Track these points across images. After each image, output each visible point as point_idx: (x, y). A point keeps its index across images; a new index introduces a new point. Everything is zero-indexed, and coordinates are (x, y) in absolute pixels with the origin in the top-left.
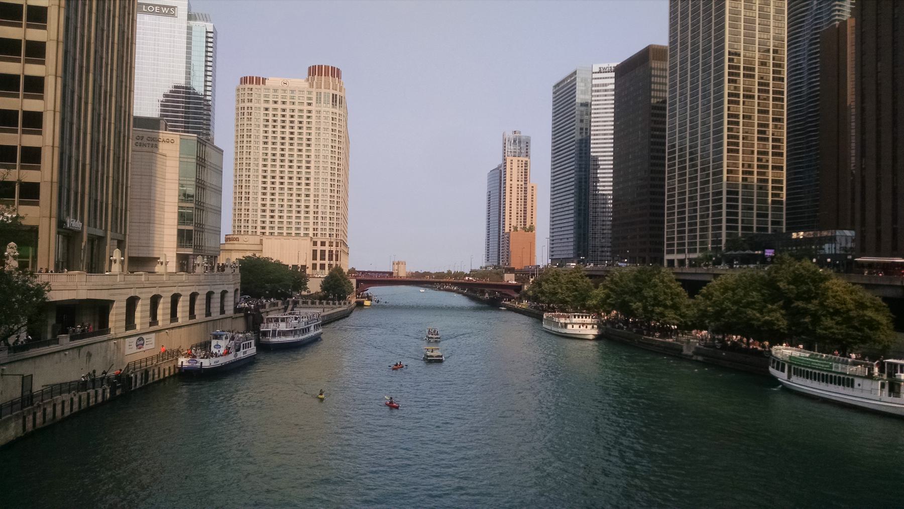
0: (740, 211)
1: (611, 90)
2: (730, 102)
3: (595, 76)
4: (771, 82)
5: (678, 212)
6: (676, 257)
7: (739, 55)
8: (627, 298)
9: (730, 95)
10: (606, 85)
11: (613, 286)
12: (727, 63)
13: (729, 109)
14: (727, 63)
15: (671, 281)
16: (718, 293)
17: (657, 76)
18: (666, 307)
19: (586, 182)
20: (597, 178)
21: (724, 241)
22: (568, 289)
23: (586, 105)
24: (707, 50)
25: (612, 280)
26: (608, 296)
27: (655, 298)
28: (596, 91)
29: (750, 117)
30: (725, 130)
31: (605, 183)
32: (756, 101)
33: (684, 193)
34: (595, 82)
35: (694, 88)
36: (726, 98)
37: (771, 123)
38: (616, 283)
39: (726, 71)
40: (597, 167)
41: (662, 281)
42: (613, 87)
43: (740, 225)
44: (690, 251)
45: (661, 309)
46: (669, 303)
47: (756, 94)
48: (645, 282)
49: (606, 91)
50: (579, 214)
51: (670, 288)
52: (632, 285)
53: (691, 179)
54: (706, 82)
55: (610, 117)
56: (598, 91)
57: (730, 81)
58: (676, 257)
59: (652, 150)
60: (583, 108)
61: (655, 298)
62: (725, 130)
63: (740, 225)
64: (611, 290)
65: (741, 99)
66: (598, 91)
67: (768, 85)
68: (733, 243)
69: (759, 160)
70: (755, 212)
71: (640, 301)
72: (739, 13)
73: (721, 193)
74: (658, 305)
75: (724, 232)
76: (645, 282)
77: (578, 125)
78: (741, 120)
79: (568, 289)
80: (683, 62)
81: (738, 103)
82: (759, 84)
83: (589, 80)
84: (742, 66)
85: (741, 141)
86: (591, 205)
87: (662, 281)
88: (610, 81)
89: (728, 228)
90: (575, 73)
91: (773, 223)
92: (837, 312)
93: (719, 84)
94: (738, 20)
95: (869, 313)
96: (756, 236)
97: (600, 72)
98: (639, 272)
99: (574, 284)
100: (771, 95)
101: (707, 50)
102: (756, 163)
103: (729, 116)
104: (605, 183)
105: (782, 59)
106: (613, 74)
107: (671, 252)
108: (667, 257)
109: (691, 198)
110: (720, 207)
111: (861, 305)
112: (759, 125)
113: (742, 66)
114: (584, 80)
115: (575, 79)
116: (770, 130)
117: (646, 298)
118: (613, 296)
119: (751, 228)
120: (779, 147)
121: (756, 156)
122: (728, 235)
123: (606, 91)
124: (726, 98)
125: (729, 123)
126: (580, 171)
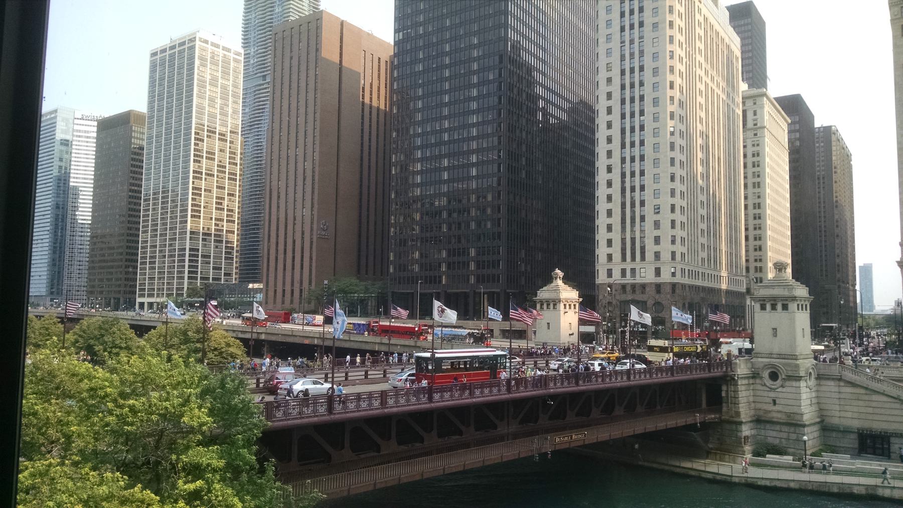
0: (199, 264)
1: (93, 138)
2: (194, 177)
3: (76, 121)
4: (227, 165)
5: (170, 239)
6: (146, 300)
7: (203, 141)
8: (92, 342)
9: (194, 172)
10: (88, 132)
11: (82, 333)
12: (193, 147)
13: (193, 183)
14: (193, 147)
15: (126, 330)
16: (154, 339)
17: (137, 138)
18: (121, 348)
19: (63, 221)
20: (75, 215)
21: (185, 289)
22: (40, 334)
23: (66, 143)
24: (178, 131)
25: (80, 329)
26: (77, 341)
27: (113, 342)
28: (77, 136)
29: (210, 191)
30: (190, 199)
31: (84, 213)
32: (215, 178)
33: (155, 246)
34: (76, 127)
35: (167, 160)
36: (191, 174)
37: (226, 197)
38: (84, 332)
39: (192, 152)
40: (76, 196)
41: (119, 330)
42: (95, 135)
43: (199, 276)
44: (158, 296)
45: (118, 350)
46: (123, 345)
47: (216, 174)
48: (107, 330)
49: (88, 137)
50: (54, 252)
51: (125, 334)
52: (96, 332)
53: (161, 235)
54: (176, 158)
55: (91, 163)
56: (79, 136)
57: (195, 161)
58: (146, 300)
59: (130, 203)
60: (63, 148)
61: (113, 342)
62: (190, 199)
63: (199, 276)
64: (80, 336)
65: (204, 176)
66: (79, 136)
67: (225, 167)
68: (192, 292)
69: (216, 225)
70: (211, 265)
71: (102, 344)
72: (204, 108)
73: (185, 249)
74: (116, 347)
75: (186, 280)
76: (107, 330)
77: (57, 163)
78: (203, 193)
79: (40, 334)
80: (159, 136)
81: (201, 179)
82: (218, 166)
83: (71, 121)
84: (205, 150)
85: (202, 209)
86: (67, 244)
87: (119, 330)
88: (92, 130)
89: (189, 278)
90: (56, 111)
91: (225, 274)
92: (216, 349)
93: (187, 162)
94: (203, 114)
95: (231, 349)
96: (211, 284)
97: (82, 119)
98: (103, 322)
99: (47, 329)
100: (227, 176)
101: (178, 131)
102: (213, 227)
103: (194, 188)
104: (84, 213)
105: (236, 149)
106: (95, 123)
107: (142, 296)
108: (139, 300)
109: (161, 251)
110: (184, 261)
111: (228, 345)
112: (217, 198)
113: (205, 150)
114: (66, 120)
115: (55, 117)
116: (226, 202)
117: (106, 343)
118: (80, 340)
119: (208, 279)
120: (232, 216)
121: (214, 222)
122: (189, 283)
123: (88, 137)
124: (191, 174)
125: (193, 194)
126: (57, 197)
